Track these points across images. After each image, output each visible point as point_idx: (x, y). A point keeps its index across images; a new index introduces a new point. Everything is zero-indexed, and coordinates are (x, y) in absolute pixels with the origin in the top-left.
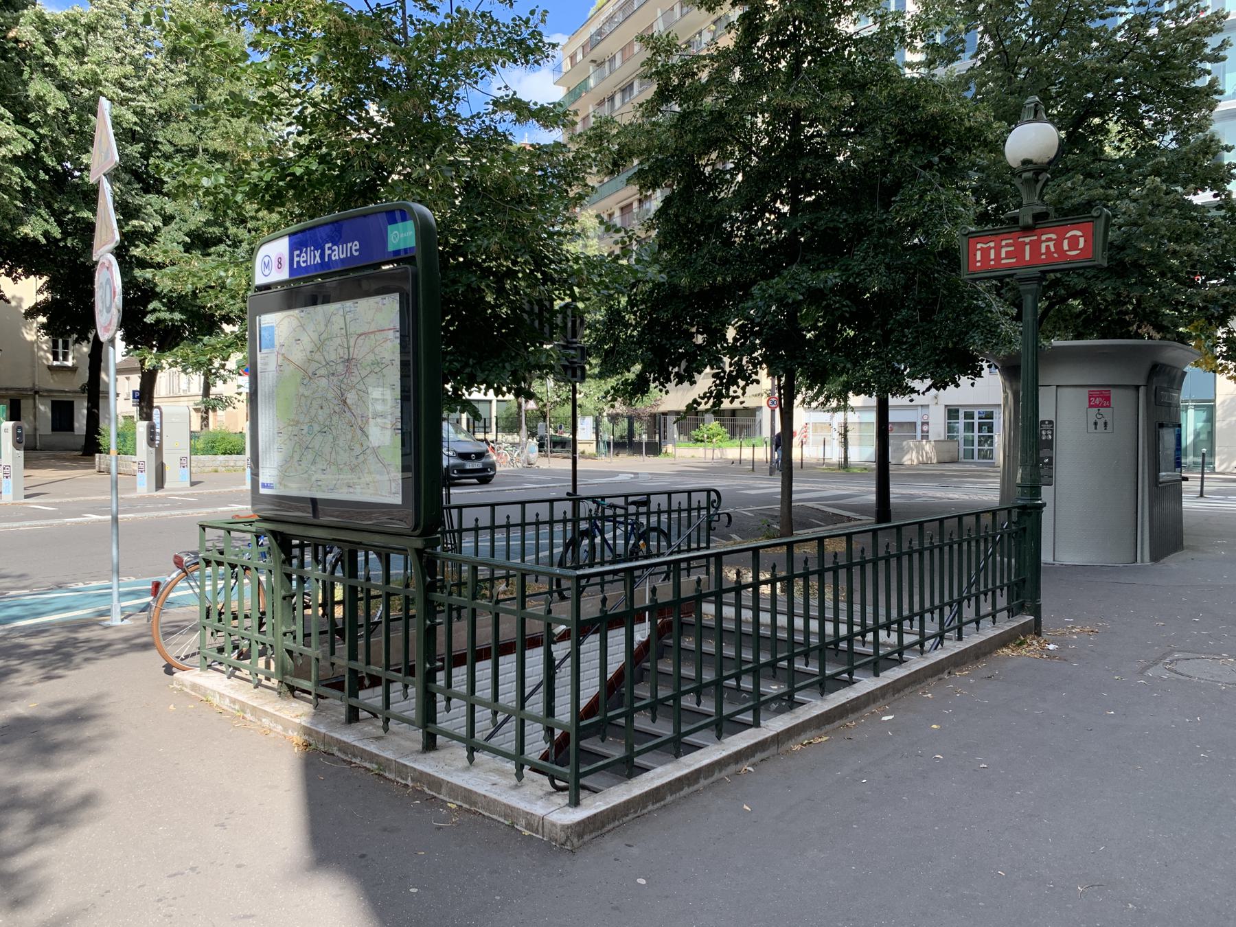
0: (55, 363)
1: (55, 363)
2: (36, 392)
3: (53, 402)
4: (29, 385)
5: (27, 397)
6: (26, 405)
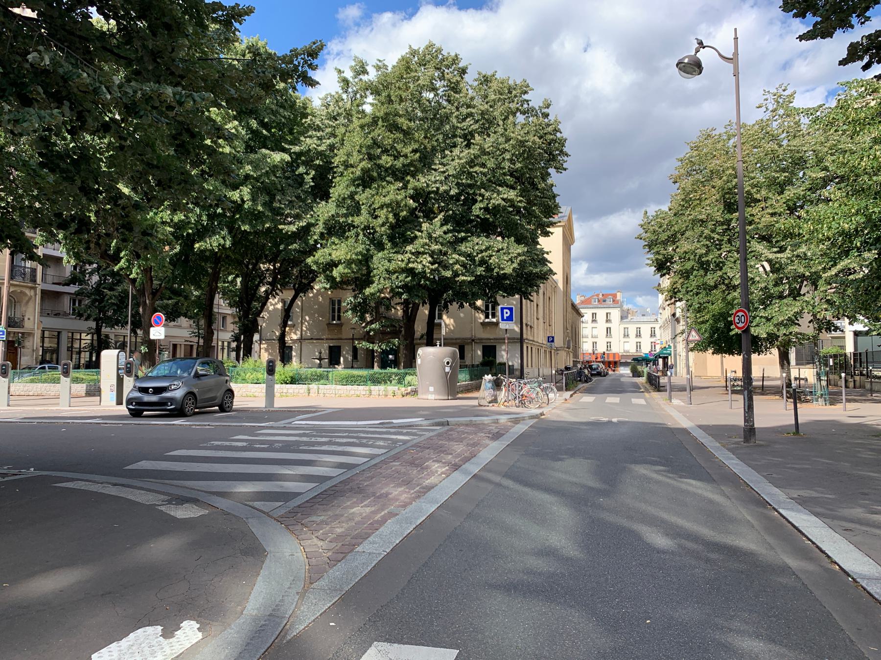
0: (487, 320)
1: (487, 320)
2: (473, 340)
3: (483, 346)
4: (469, 336)
5: (468, 344)
6: (467, 348)
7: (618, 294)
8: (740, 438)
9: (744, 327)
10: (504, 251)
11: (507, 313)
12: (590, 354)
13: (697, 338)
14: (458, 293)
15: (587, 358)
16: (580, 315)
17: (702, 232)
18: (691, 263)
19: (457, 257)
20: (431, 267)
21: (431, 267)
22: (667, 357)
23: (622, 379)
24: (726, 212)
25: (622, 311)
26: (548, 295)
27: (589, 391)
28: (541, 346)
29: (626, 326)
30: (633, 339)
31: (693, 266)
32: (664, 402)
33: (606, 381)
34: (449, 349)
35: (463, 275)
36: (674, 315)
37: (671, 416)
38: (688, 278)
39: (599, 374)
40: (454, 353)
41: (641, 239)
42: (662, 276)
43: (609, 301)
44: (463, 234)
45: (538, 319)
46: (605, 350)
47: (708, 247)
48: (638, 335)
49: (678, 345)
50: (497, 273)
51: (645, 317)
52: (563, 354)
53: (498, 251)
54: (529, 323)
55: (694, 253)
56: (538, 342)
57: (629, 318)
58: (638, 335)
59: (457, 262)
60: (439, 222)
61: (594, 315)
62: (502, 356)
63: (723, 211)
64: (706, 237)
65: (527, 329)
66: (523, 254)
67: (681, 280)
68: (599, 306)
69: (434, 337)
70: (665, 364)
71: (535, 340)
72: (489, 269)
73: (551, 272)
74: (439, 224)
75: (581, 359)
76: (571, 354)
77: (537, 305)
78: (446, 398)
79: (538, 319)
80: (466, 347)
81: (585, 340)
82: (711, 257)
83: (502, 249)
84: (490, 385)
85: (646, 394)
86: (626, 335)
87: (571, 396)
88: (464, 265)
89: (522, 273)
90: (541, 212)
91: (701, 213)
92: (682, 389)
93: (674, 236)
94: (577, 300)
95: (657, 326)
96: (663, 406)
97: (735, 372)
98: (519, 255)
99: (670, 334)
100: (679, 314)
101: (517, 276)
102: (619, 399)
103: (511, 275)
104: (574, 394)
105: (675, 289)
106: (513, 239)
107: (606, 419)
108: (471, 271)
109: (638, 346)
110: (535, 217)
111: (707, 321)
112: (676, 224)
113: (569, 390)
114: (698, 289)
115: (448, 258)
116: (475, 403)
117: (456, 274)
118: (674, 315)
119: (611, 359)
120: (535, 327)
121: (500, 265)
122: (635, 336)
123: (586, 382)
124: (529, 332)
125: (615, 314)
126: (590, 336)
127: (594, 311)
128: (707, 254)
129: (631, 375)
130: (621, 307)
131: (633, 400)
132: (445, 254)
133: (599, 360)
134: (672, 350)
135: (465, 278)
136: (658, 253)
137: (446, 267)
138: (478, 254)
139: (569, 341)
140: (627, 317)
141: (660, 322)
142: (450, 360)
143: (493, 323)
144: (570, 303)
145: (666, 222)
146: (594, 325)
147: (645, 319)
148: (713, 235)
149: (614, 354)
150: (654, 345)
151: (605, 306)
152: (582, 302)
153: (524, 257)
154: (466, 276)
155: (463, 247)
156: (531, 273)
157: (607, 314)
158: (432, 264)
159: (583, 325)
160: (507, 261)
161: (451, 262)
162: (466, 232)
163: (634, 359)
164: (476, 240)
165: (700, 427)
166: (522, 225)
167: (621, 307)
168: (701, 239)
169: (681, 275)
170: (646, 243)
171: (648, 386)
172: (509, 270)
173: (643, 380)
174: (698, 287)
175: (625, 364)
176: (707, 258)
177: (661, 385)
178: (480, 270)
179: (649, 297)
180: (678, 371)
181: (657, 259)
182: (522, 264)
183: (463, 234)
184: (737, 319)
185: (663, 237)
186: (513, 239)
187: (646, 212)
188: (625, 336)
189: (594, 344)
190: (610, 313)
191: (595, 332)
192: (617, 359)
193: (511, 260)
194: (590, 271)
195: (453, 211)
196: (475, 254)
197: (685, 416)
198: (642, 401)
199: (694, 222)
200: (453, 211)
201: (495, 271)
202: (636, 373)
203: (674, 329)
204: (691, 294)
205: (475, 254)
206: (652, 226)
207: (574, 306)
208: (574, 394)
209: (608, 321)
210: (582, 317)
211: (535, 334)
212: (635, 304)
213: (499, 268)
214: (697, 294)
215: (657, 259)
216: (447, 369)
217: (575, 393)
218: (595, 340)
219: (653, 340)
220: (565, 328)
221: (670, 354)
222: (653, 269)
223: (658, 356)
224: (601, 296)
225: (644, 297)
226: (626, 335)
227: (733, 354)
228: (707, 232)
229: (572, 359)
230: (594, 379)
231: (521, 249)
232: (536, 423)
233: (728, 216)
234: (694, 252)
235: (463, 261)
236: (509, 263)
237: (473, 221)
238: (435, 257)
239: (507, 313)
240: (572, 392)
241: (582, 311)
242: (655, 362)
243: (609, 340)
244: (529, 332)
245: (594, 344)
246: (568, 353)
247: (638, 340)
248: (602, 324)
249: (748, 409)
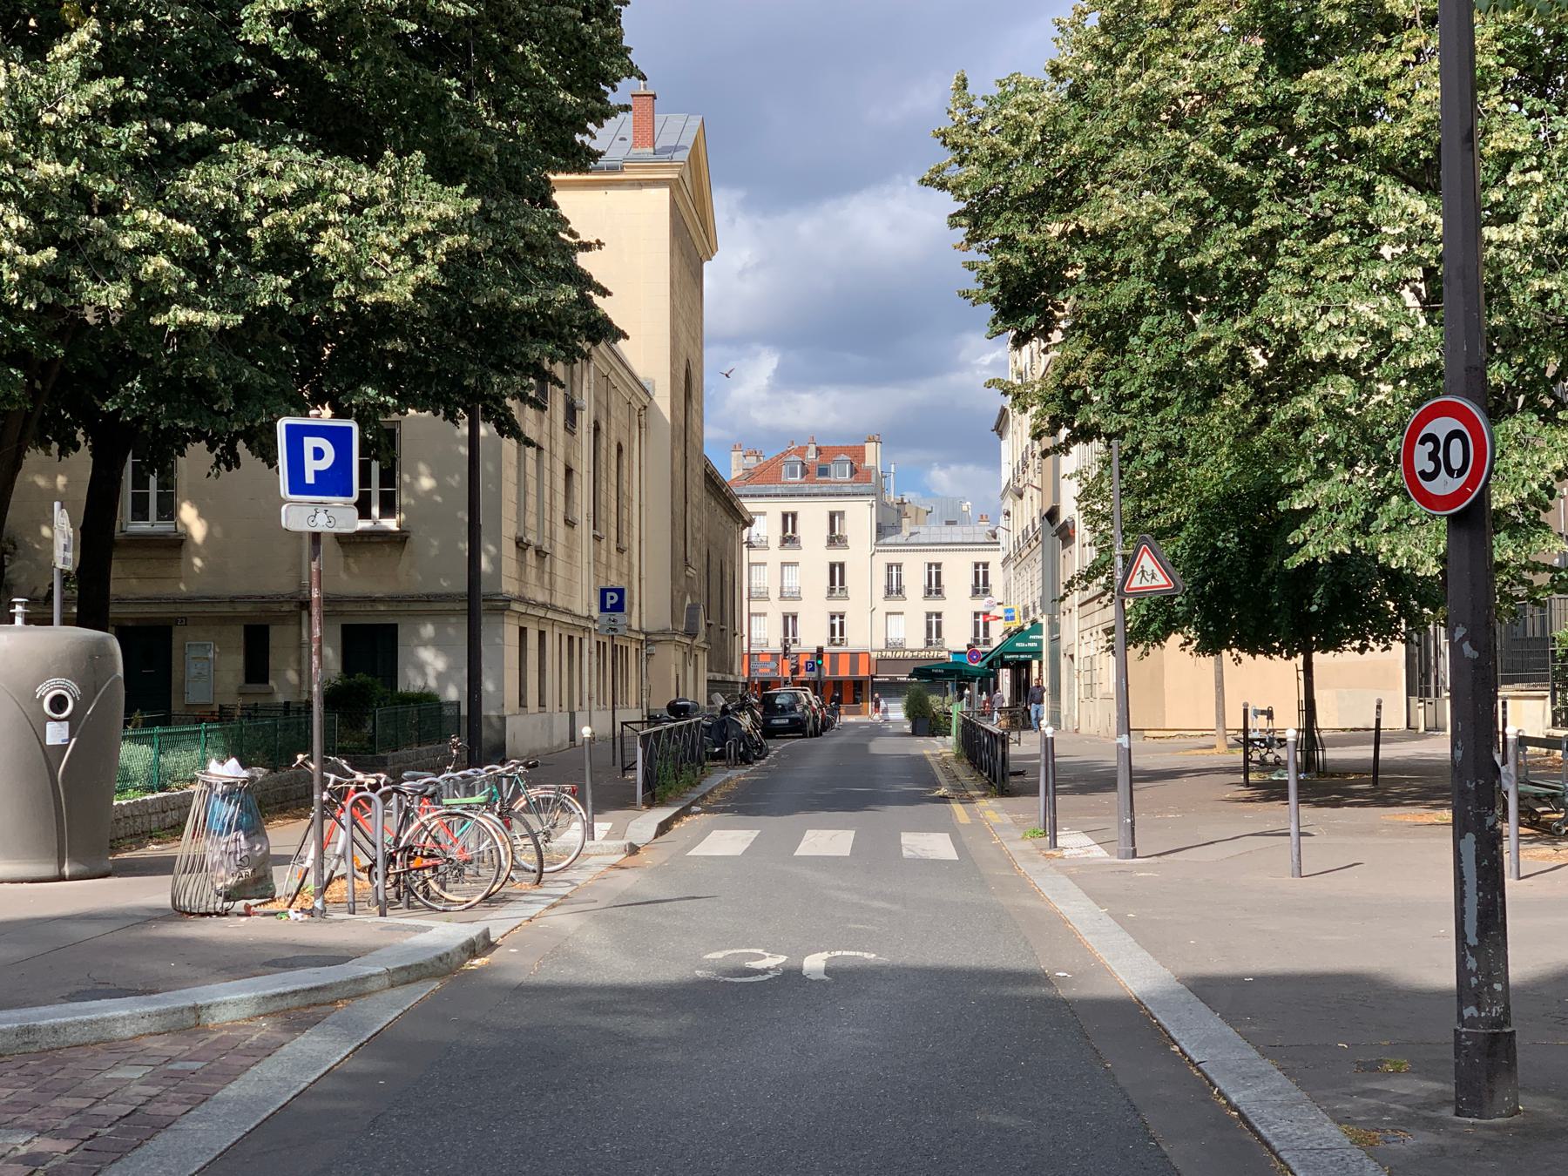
3: (345, 628)
5: (282, 619)
7: (870, 449)
8: (1423, 1070)
9: (1460, 495)
10: (382, 209)
11: (318, 454)
12: (774, 656)
13: (1161, 581)
14: (173, 384)
15: (764, 671)
16: (744, 521)
17: (1180, 153)
18: (1136, 284)
19: (157, 219)
20: (24, 259)
21: (24, 259)
22: (1027, 665)
23: (878, 747)
24: (1272, 70)
25: (882, 507)
26: (614, 432)
27: (743, 804)
28: (581, 625)
29: (894, 558)
30: (916, 604)
31: (1140, 298)
32: (1027, 845)
33: (816, 755)
34: (64, 638)
35: (189, 302)
36: (1051, 515)
37: (1062, 921)
38: (1119, 346)
39: (797, 728)
40: (93, 660)
41: (942, 186)
42: (1020, 341)
43: (840, 473)
44: (197, 128)
45: (570, 523)
46: (824, 643)
47: (1203, 214)
48: (934, 588)
49: (1064, 621)
50: (349, 301)
51: (955, 528)
52: (670, 658)
53: (357, 207)
54: (531, 537)
55: (1145, 234)
56: (568, 612)
57: (905, 533)
58: (934, 588)
59: (160, 243)
60: (76, 63)
61: (789, 519)
62: (421, 667)
63: (1263, 67)
64: (1194, 171)
65: (522, 562)
66: (466, 223)
67: (1096, 355)
68: (807, 488)
69: (114, 588)
70: (1022, 688)
71: (559, 602)
72: (314, 287)
73: (604, 331)
74: (72, 69)
75: (741, 673)
76: (703, 659)
77: (569, 471)
78: (50, 869)
79: (570, 523)
80: (273, 631)
81: (756, 607)
82: (1215, 252)
83: (373, 201)
84: (227, 811)
85: (957, 808)
86: (894, 590)
87: (664, 828)
88: (195, 265)
89: (462, 311)
90: (551, 68)
91: (1175, 72)
92: (1093, 781)
93: (1071, 174)
94: (732, 469)
95: (994, 559)
96: (1024, 867)
97: (1269, 714)
98: (446, 226)
99: (1038, 584)
100: (1069, 510)
101: (444, 318)
102: (850, 835)
103: (408, 313)
104: (676, 817)
105: (1068, 390)
106: (418, 157)
107: (772, 961)
108: (230, 290)
109: (934, 625)
110: (527, 84)
111: (1178, 526)
112: (1076, 130)
113: (663, 803)
114: (1159, 387)
115: (114, 224)
116: (152, 893)
117: (150, 298)
118: (1051, 515)
119: (844, 672)
120: (560, 551)
121: (359, 267)
122: (922, 592)
123: (745, 759)
124: (532, 574)
125: (860, 516)
126: (774, 594)
127: (789, 506)
128: (1194, 243)
129: (908, 728)
130: (878, 492)
131: (907, 839)
132: (109, 208)
133: (803, 675)
134: (1045, 637)
135: (193, 316)
136: (1008, 242)
137: (105, 267)
138: (261, 213)
139: (693, 609)
140: (897, 529)
141: (1003, 543)
142: (70, 690)
143: (386, 534)
144: (699, 470)
145: (1040, 119)
146: (789, 555)
147: (956, 534)
148: (1223, 163)
149: (855, 656)
150: (982, 621)
151: (825, 489)
152: (750, 475)
153: (463, 239)
154: (203, 308)
155: (191, 183)
156: (498, 315)
157: (832, 516)
158: (32, 246)
159: (748, 556)
160: (394, 255)
161: (127, 242)
162: (213, 118)
163: (919, 673)
164: (254, 154)
165: (1206, 989)
166: (470, 116)
167: (878, 492)
168: (1175, 179)
169: (1094, 335)
170: (962, 206)
171: (963, 771)
172: (398, 290)
173: (944, 747)
174: (1165, 377)
175: (891, 689)
176: (1199, 258)
177: (1013, 765)
178: (271, 288)
179: (970, 469)
180: (1064, 712)
181: (1004, 268)
182: (459, 266)
183: (197, 128)
184: (1422, 453)
185: (1029, 178)
186: (418, 157)
187: (963, 84)
188: (889, 591)
189: (790, 620)
190: (842, 514)
191: (793, 580)
192: (863, 673)
193: (409, 246)
194: (786, 379)
195: (148, 20)
196: (248, 215)
197: (1120, 919)
198: (938, 846)
199: (1148, 107)
200: (148, 20)
201: (339, 291)
202: (925, 723)
203: (1051, 569)
204: (1135, 405)
205: (248, 215)
206: (984, 134)
207: (714, 483)
208: (676, 817)
209: (835, 540)
210: (749, 524)
211: (559, 582)
212: (926, 492)
213: (356, 281)
214: (1157, 405)
215: (1004, 268)
216: (56, 734)
217: (685, 812)
218: (790, 607)
219: (981, 605)
220: (680, 561)
221: (1037, 653)
222: (989, 311)
223: (998, 661)
224: (811, 455)
225: (954, 468)
226: (894, 590)
227: (1269, 652)
228: (1199, 149)
229: (704, 675)
230: (776, 747)
231: (450, 203)
232: (436, 996)
233: (1279, 88)
234: (1147, 228)
235: (182, 236)
236: (404, 261)
237: (235, 74)
238: (51, 215)
239: (318, 454)
240: (664, 813)
241: (750, 505)
242: (988, 683)
243: (837, 606)
244: (532, 574)
245: (790, 620)
246: (689, 654)
247: (934, 605)
248: (814, 553)
249: (1482, 932)
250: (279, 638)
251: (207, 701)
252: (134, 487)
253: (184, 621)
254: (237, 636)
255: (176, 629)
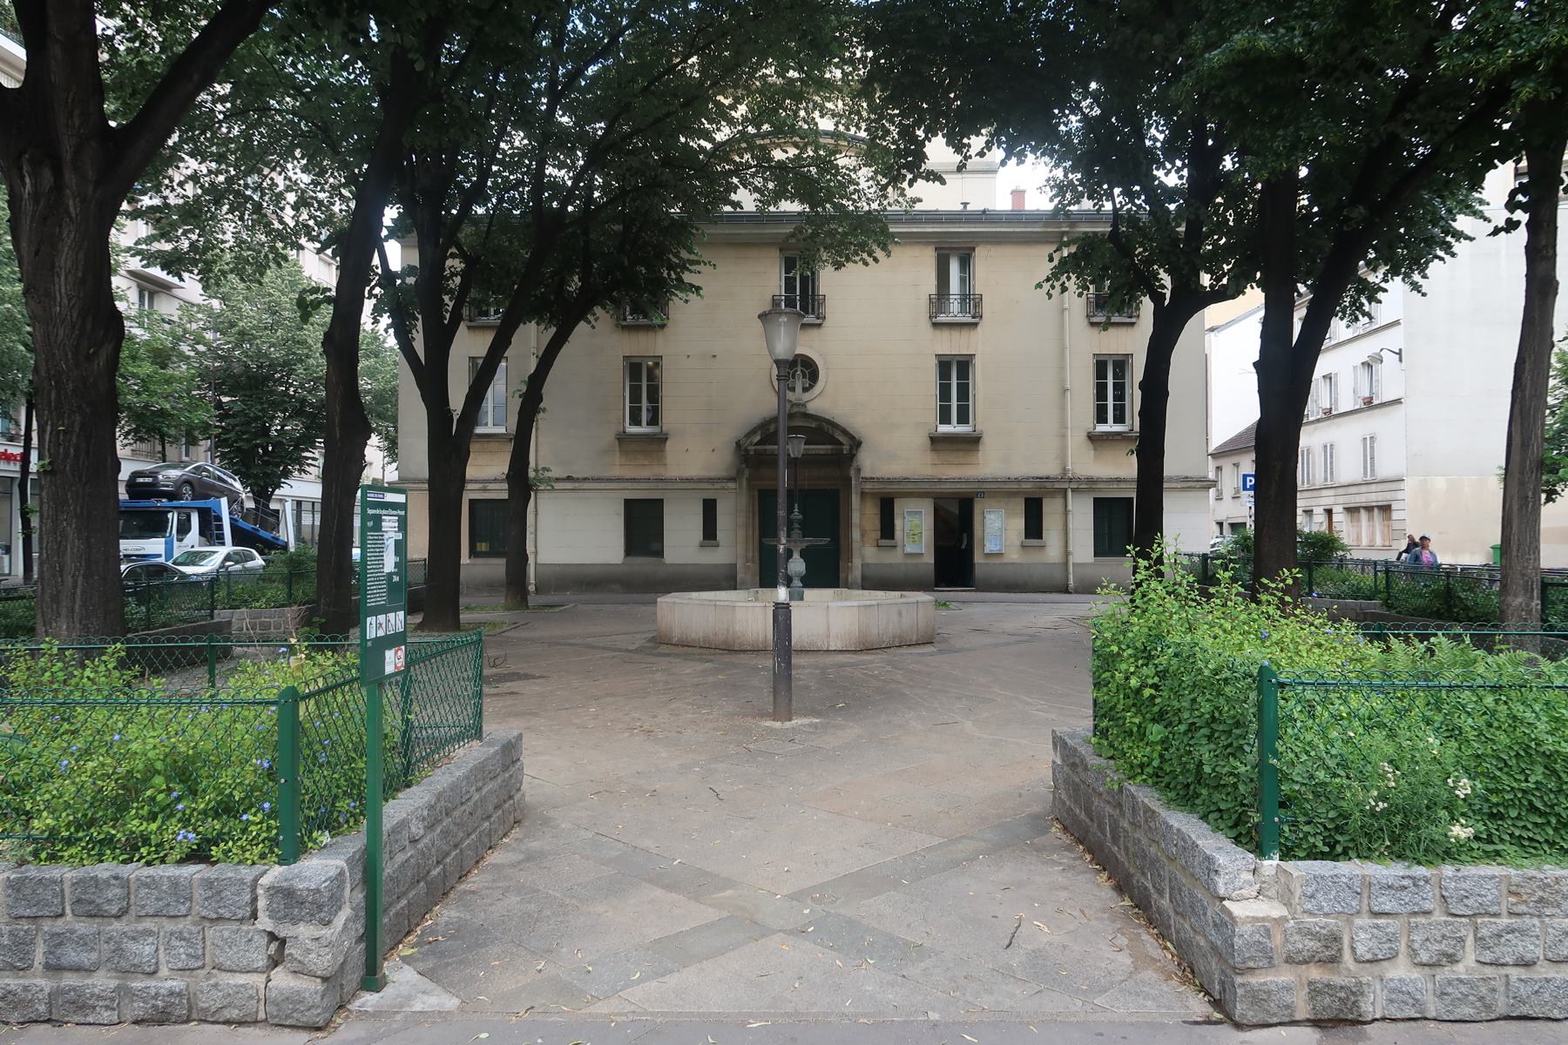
3: (1095, 500)
5: (1054, 493)
250: (1051, 510)
251: (919, 552)
252: (640, 408)
253: (982, 494)
254: (1020, 506)
255: (976, 500)
